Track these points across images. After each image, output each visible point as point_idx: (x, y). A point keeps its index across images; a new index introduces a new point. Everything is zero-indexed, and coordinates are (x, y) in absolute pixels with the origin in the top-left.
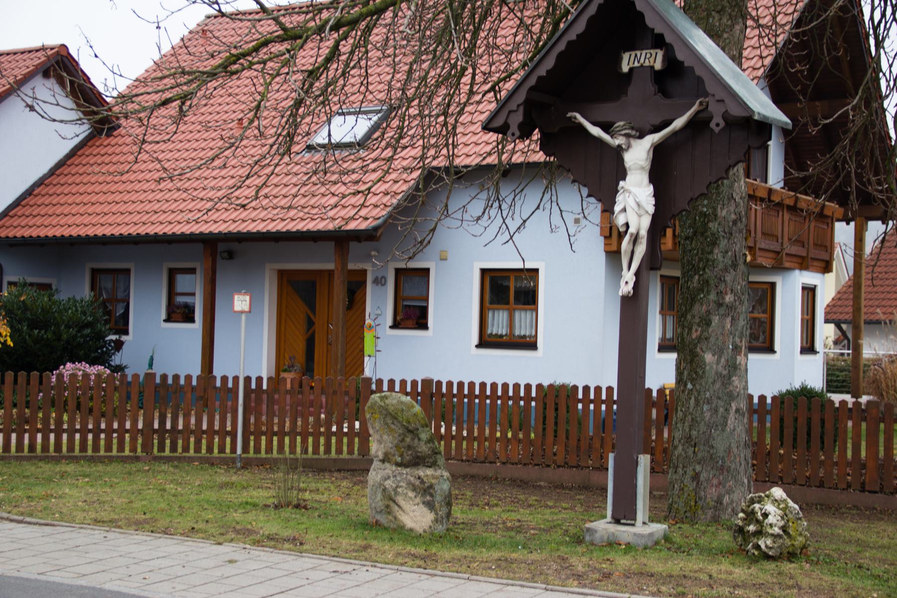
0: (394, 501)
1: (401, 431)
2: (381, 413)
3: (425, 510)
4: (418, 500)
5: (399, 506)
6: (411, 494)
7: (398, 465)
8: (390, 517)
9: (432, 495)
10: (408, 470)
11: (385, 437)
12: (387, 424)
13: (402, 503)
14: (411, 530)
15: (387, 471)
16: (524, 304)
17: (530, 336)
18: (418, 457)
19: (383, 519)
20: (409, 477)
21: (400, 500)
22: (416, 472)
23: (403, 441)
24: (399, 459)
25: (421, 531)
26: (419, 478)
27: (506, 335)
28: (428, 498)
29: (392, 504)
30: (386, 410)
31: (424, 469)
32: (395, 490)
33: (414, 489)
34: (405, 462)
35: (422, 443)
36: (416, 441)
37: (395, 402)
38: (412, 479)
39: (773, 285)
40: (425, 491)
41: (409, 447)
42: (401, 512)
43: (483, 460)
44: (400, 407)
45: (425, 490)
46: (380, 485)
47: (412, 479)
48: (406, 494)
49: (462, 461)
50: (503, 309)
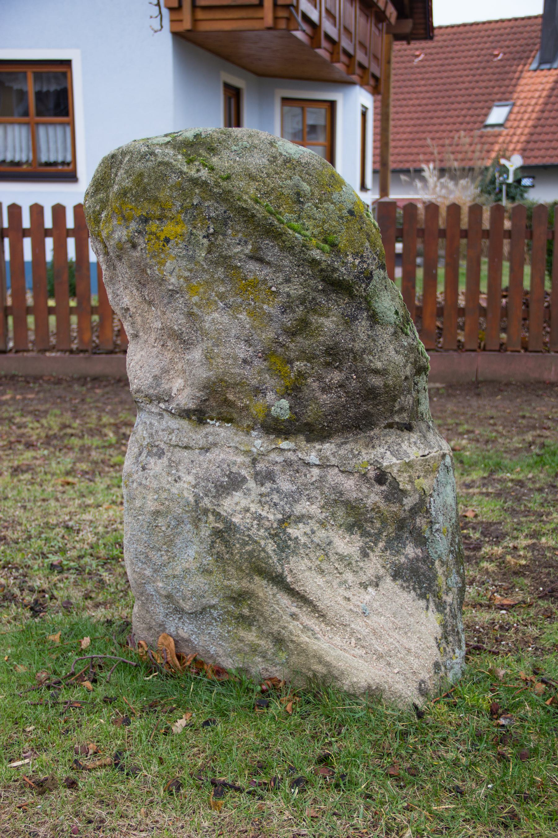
0: (279, 581)
1: (295, 290)
2: (193, 212)
3: (400, 599)
4: (374, 565)
5: (302, 598)
6: (346, 544)
7: (275, 428)
8: (251, 636)
9: (421, 541)
10: (328, 447)
11: (215, 318)
12: (225, 261)
13: (312, 583)
14: (374, 694)
15: (216, 455)
16: (56, 115)
17: (63, 163)
18: (371, 394)
19: (216, 643)
20: (334, 477)
21: (303, 571)
22: (367, 455)
23: (302, 327)
24: (282, 407)
25: (409, 693)
26: (381, 477)
27: (27, 162)
28: (411, 551)
29: (263, 589)
30: (225, 197)
31: (392, 437)
32: (278, 533)
33: (356, 519)
34: (310, 413)
35: (385, 334)
36: (362, 326)
37: (257, 161)
38: (349, 484)
39: (332, 105)
40: (401, 524)
41: (334, 355)
42: (311, 622)
43: (110, 347)
44: (288, 183)
45: (391, 521)
46: (198, 514)
47: (349, 484)
48: (325, 548)
49: (71, 352)
50: (20, 123)
